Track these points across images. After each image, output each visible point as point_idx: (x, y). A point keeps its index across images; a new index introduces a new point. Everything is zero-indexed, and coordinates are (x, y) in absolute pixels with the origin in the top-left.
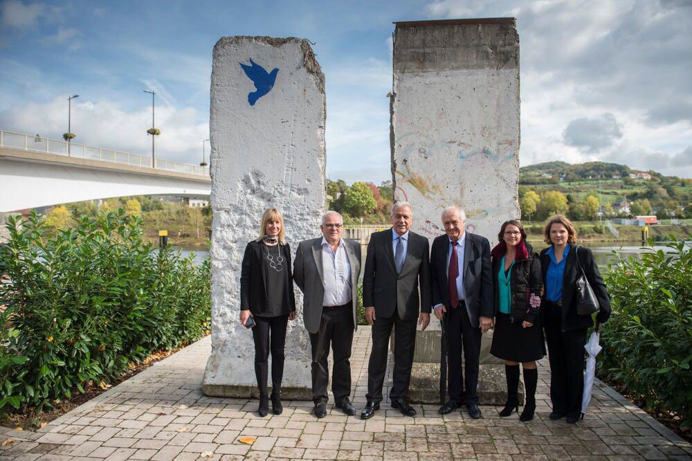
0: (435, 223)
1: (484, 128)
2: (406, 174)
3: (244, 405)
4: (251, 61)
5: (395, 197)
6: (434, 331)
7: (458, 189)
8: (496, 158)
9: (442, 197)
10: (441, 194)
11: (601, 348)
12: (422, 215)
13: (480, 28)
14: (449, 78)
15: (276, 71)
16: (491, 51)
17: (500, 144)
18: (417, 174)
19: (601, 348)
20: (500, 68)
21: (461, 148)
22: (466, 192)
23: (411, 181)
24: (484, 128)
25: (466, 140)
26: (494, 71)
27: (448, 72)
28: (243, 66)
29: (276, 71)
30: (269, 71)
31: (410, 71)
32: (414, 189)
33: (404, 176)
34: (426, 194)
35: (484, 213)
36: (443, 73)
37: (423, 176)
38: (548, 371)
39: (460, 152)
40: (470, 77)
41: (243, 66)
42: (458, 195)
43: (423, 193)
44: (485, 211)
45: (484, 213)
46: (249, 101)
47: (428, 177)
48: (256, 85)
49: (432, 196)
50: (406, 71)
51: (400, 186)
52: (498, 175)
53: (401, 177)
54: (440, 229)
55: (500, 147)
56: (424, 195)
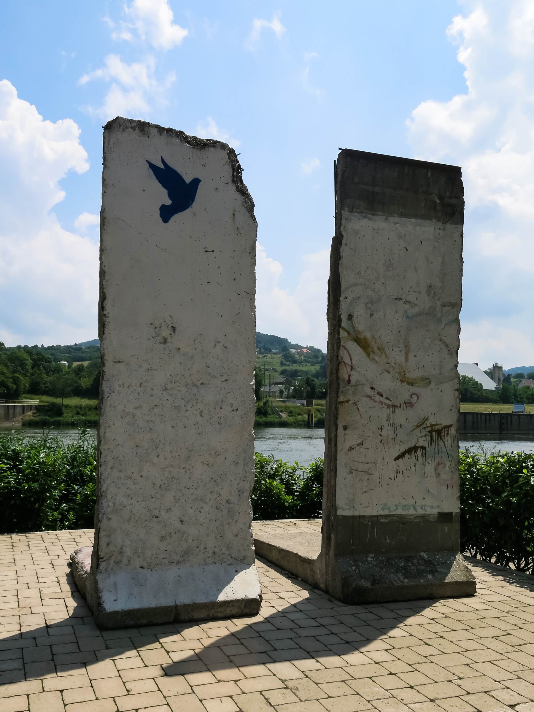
0: (380, 390)
1: (430, 287)
2: (352, 331)
3: (300, 590)
4: (163, 161)
5: (340, 358)
6: (378, 516)
7: (403, 353)
8: (439, 320)
9: (388, 361)
10: (386, 356)
11: (70, 569)
12: (367, 380)
13: (429, 174)
14: (398, 226)
15: (196, 182)
16: (439, 202)
17: (444, 306)
18: (332, 313)
19: (70, 569)
20: (446, 223)
21: (407, 306)
22: (411, 355)
23: (357, 340)
24: (430, 287)
25: (412, 298)
26: (440, 225)
27: (397, 219)
28: (152, 166)
29: (196, 182)
30: (188, 179)
31: (358, 210)
32: (359, 350)
33: (349, 333)
34: (371, 356)
35: (427, 381)
36: (392, 219)
37: (368, 335)
38: (262, 607)
39: (406, 311)
40: (418, 228)
41: (152, 166)
42: (403, 359)
43: (368, 355)
44: (428, 379)
45: (427, 381)
46: (162, 215)
47: (374, 337)
48: (170, 195)
49: (376, 358)
50: (355, 210)
51: (344, 344)
52: (441, 340)
53: (346, 334)
54: (385, 396)
55: (444, 308)
56: (369, 357)
